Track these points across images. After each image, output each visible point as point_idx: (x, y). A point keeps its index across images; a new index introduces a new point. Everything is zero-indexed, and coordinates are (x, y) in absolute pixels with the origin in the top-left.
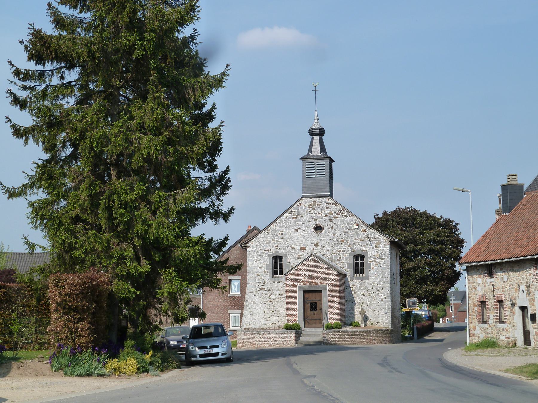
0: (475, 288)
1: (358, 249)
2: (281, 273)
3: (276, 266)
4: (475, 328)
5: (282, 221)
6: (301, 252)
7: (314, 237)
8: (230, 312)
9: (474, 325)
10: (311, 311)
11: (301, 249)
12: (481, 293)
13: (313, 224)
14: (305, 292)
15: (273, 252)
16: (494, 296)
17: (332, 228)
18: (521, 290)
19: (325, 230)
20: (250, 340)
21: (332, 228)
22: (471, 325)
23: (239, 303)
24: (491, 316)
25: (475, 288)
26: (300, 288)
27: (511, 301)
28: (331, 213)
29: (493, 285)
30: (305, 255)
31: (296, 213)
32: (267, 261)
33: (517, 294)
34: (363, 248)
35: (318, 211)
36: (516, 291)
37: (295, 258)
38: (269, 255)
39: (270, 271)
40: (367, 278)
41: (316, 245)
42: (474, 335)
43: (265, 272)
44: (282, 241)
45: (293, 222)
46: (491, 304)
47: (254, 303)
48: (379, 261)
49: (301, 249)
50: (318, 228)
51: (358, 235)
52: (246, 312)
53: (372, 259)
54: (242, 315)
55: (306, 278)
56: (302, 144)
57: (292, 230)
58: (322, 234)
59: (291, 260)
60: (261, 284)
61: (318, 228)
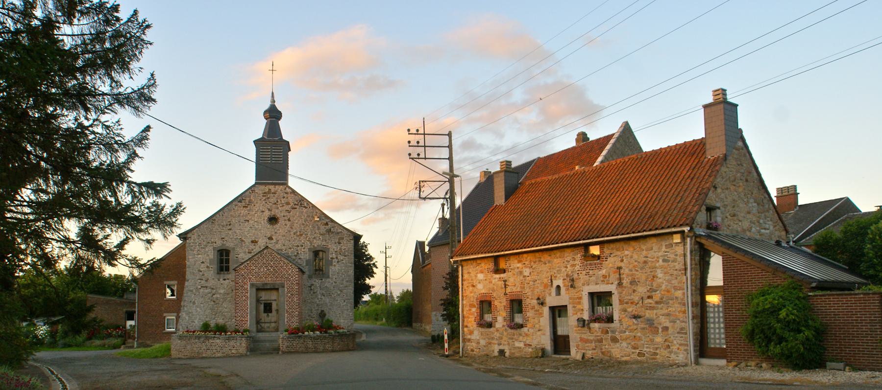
0: (473, 286)
1: (318, 243)
2: (227, 269)
3: (221, 261)
4: (471, 333)
5: (230, 210)
6: (252, 246)
7: (268, 230)
8: (165, 314)
9: (471, 328)
10: (265, 312)
11: (256, 242)
12: (483, 291)
13: (267, 214)
14: (258, 290)
15: (219, 244)
16: (505, 294)
17: (289, 220)
18: (555, 285)
19: (281, 221)
20: (189, 347)
21: (289, 220)
22: (465, 329)
23: (176, 307)
24: (500, 319)
25: (473, 286)
26: (252, 285)
27: (538, 299)
28: (288, 204)
29: (505, 281)
30: (257, 249)
31: (247, 201)
32: (211, 254)
33: (547, 291)
34: (324, 243)
35: (273, 200)
36: (546, 286)
37: (245, 252)
38: (214, 249)
39: (215, 267)
40: (328, 277)
41: (271, 238)
42: (469, 340)
43: (208, 267)
44: (230, 232)
45: (244, 212)
46: (501, 305)
47: (194, 303)
48: (341, 257)
49: (252, 242)
50: (273, 220)
51: (319, 228)
52: (183, 314)
53: (334, 256)
54: (178, 318)
55: (261, 274)
56: (259, 128)
57: (242, 220)
58: (277, 226)
59: (241, 255)
60: (203, 282)
61: (273, 220)
